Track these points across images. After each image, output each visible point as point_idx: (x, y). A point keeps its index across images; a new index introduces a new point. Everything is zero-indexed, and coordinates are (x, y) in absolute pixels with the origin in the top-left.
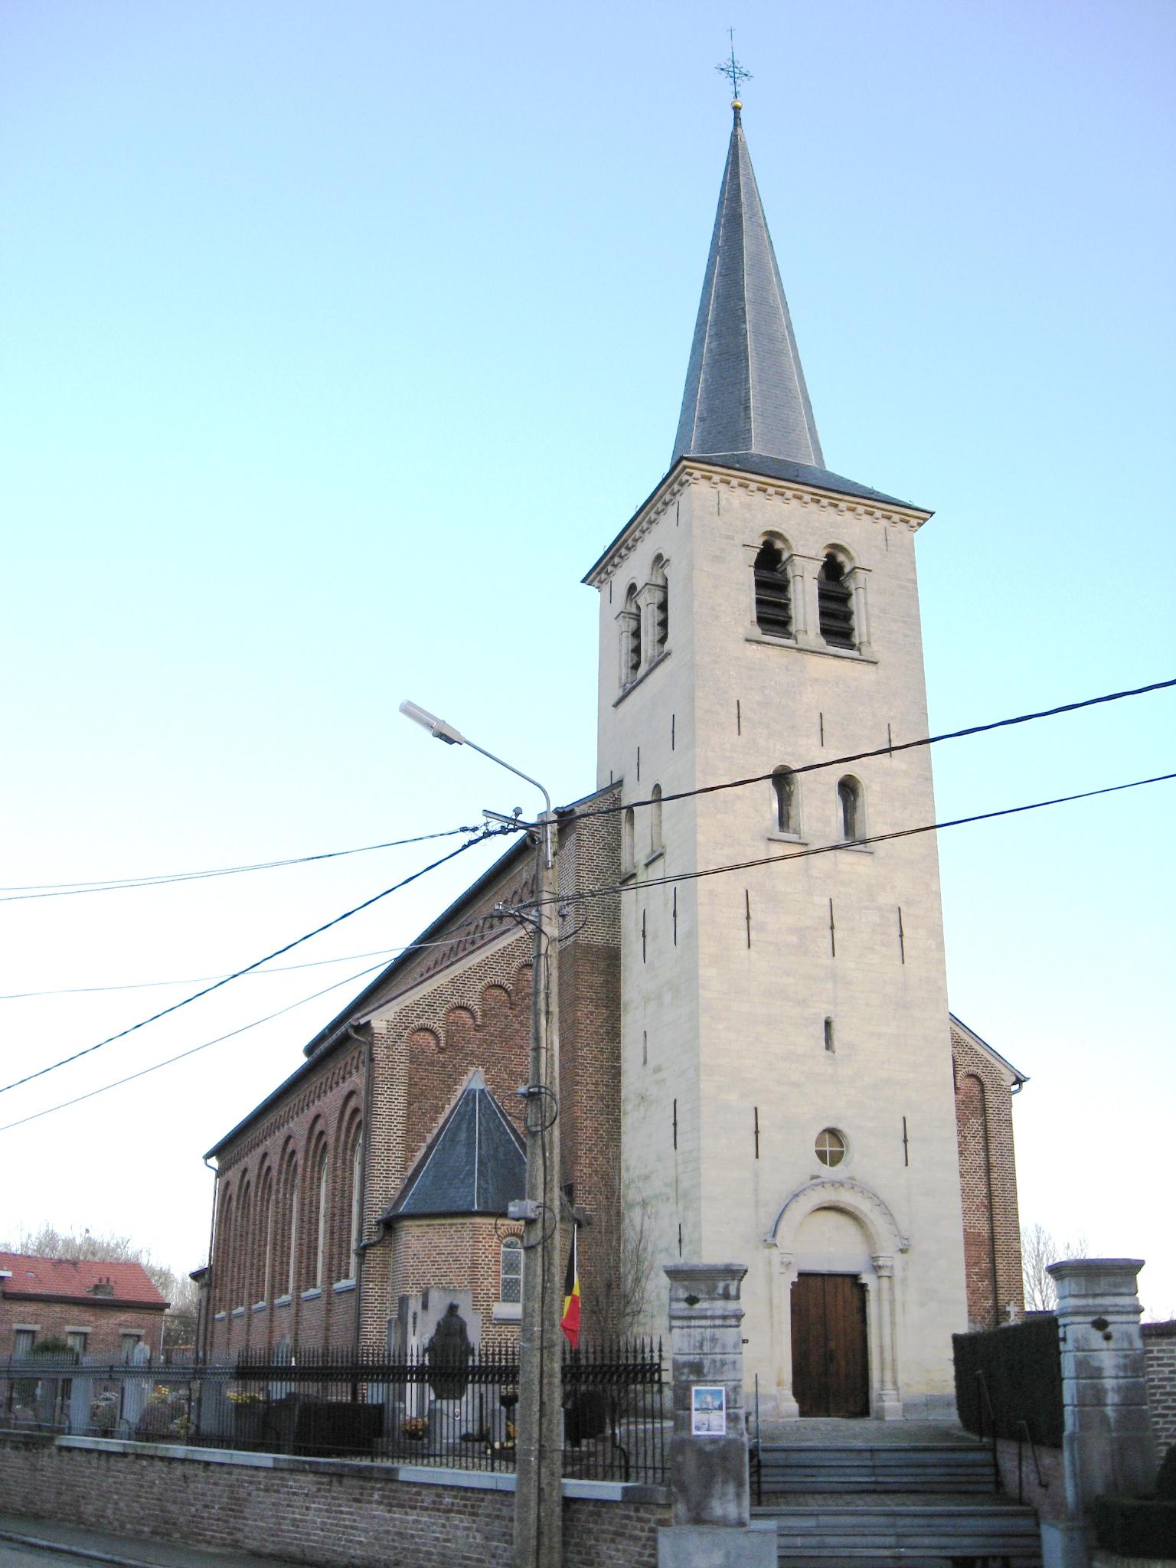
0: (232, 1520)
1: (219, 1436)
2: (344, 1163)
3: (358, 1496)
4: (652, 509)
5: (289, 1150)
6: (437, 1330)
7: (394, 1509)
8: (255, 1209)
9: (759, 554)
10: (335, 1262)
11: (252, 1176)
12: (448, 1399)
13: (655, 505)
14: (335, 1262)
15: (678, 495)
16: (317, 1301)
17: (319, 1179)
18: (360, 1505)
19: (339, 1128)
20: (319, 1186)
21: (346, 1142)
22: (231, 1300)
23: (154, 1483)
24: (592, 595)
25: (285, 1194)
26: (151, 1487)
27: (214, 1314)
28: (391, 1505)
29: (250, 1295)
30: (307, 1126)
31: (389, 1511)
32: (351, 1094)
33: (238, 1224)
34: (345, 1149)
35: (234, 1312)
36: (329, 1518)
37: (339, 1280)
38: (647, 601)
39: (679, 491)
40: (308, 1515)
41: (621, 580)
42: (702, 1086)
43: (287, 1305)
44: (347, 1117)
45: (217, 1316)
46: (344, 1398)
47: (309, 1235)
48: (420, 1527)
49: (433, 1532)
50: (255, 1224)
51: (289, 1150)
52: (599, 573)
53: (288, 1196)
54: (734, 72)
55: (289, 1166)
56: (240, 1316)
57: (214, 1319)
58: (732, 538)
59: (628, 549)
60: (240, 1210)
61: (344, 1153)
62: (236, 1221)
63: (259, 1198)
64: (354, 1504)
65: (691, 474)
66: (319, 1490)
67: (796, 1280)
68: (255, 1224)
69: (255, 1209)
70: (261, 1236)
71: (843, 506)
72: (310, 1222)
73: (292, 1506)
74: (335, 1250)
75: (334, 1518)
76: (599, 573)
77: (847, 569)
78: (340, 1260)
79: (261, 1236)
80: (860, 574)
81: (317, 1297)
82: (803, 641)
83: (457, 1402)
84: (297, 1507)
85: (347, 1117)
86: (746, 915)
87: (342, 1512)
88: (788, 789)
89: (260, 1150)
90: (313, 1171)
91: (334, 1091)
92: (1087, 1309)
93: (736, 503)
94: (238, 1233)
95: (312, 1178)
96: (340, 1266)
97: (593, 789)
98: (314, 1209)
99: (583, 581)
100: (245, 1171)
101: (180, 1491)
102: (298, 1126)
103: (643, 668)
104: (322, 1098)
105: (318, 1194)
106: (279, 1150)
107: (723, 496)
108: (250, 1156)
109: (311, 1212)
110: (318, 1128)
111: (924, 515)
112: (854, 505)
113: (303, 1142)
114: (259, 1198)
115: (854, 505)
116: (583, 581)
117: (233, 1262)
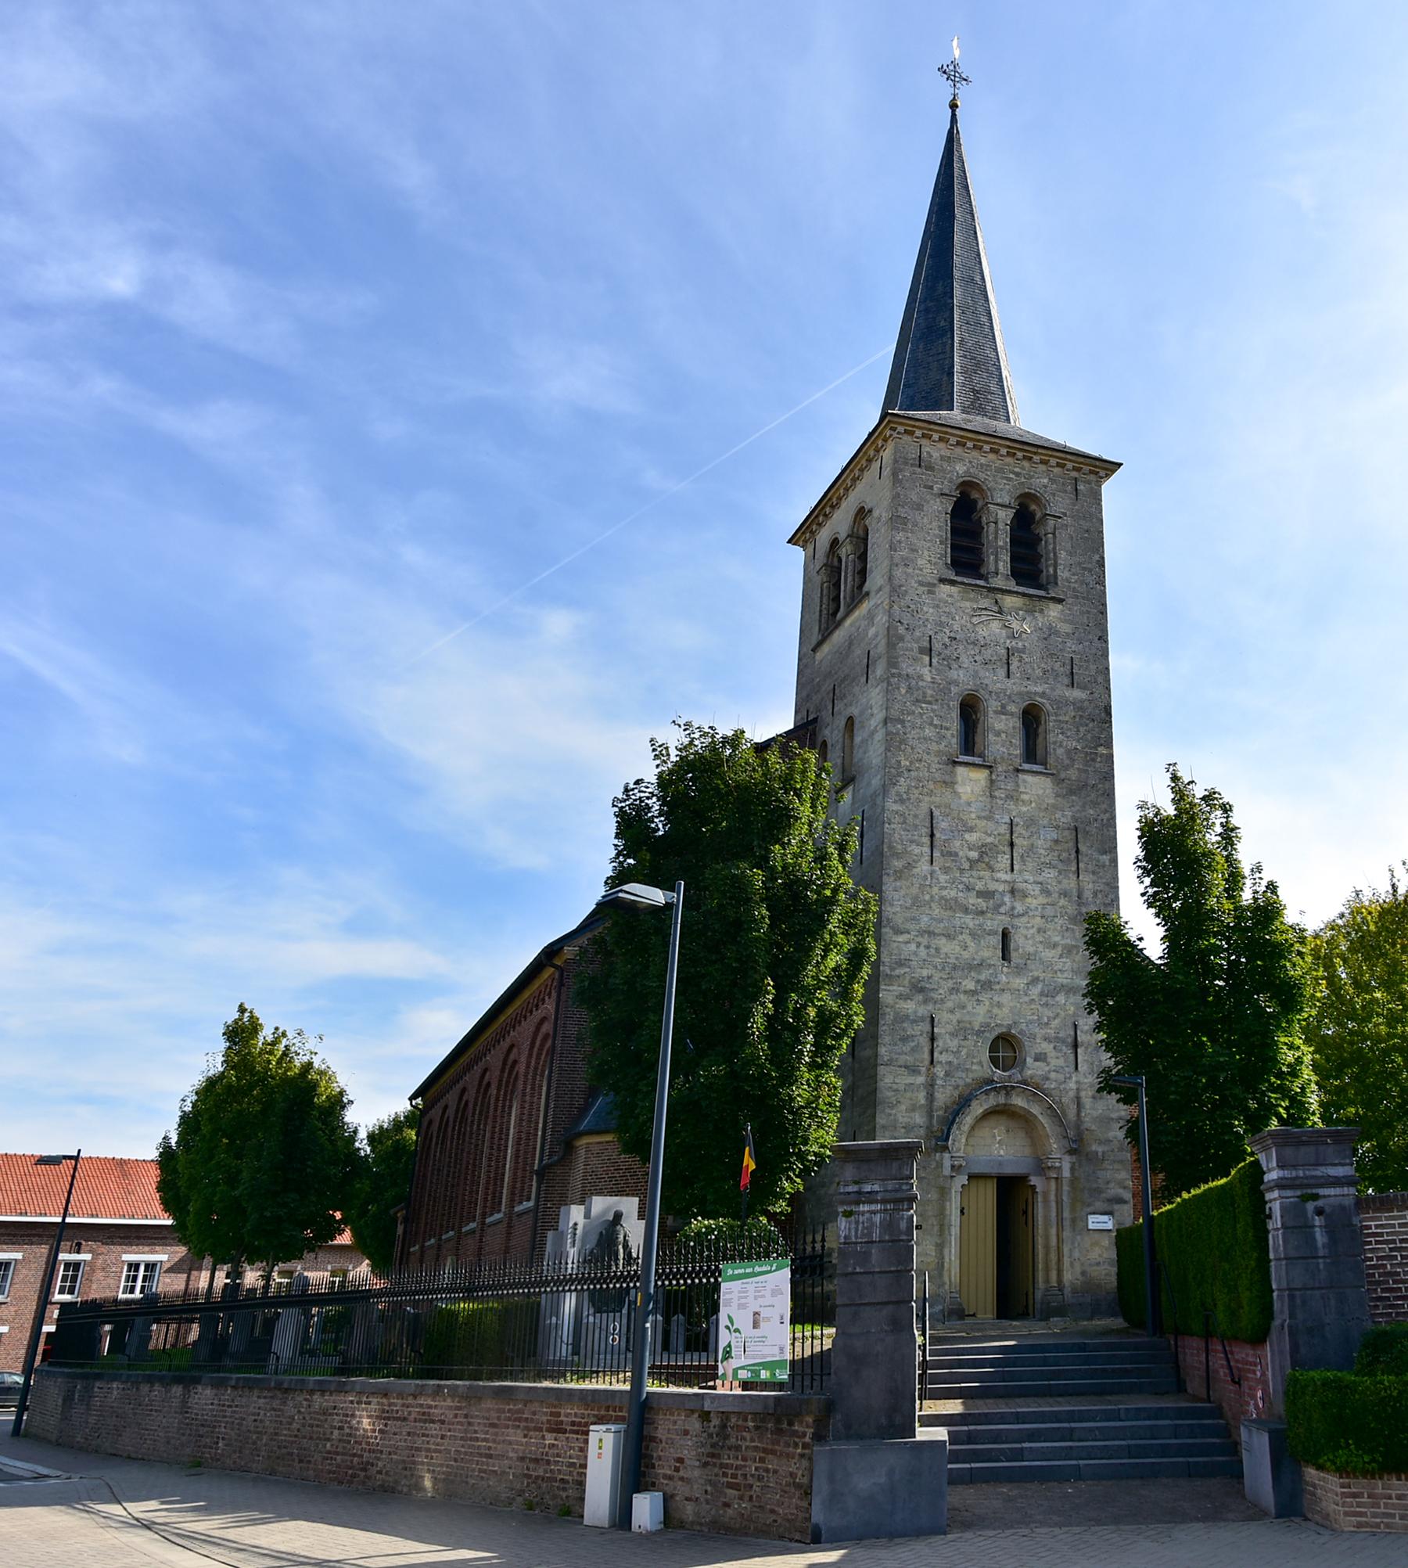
0: (366, 1454)
1: (98, 1377)
2: (533, 1089)
3: (496, 1421)
4: (856, 465)
5: (485, 1083)
6: (599, 1241)
7: (531, 1433)
8: (452, 1143)
9: (955, 502)
10: (518, 1185)
11: (451, 1112)
12: (607, 1312)
13: (858, 462)
14: (518, 1185)
15: (882, 452)
16: (500, 1226)
17: (511, 1107)
18: (496, 1430)
19: (530, 1055)
20: (510, 1114)
21: (536, 1068)
22: (425, 1232)
23: (294, 1419)
24: (798, 554)
25: (479, 1126)
26: (290, 1424)
27: (410, 1248)
28: (527, 1428)
29: (442, 1226)
30: (502, 1057)
31: (525, 1436)
32: (543, 1020)
33: (437, 1158)
34: (535, 1074)
35: (427, 1244)
36: (463, 1446)
37: (521, 1203)
38: (846, 551)
39: (882, 446)
40: (442, 1445)
41: (824, 536)
42: (881, 995)
43: (473, 1231)
44: (538, 1043)
45: (412, 1250)
46: (818, 1333)
47: (497, 1161)
48: (556, 1451)
49: (570, 1457)
50: (450, 1158)
51: (485, 1083)
52: (803, 533)
53: (482, 1127)
54: (951, 73)
55: (484, 1098)
56: (432, 1246)
57: (409, 1252)
58: (931, 488)
59: (833, 507)
60: (439, 1146)
61: (534, 1078)
62: (435, 1156)
63: (456, 1132)
64: (491, 1430)
65: (894, 429)
66: (456, 1416)
67: (1173, 796)
68: (450, 1158)
69: (452, 1143)
70: (455, 1167)
71: (1036, 458)
72: (499, 1149)
73: (427, 1436)
74: (519, 1173)
75: (470, 1447)
76: (802, 536)
77: (1038, 515)
78: (523, 1182)
79: (455, 1167)
80: (1051, 522)
81: (499, 1222)
82: (998, 582)
83: (618, 1314)
84: (432, 1436)
85: (538, 1043)
86: (930, 833)
87: (477, 1439)
88: (974, 717)
89: (459, 1086)
90: (505, 1100)
91: (528, 1020)
92: (1298, 1182)
93: (936, 455)
94: (436, 1167)
95: (503, 1106)
96: (522, 1189)
97: (791, 726)
98: (503, 1137)
99: (789, 542)
100: (446, 1107)
101: (317, 1426)
102: (494, 1059)
103: (839, 616)
104: (517, 1028)
105: (509, 1122)
106: (476, 1083)
107: (925, 449)
108: (451, 1092)
109: (500, 1139)
110: (512, 1057)
111: (1113, 467)
112: (1047, 458)
113: (498, 1073)
114: (456, 1132)
115: (1047, 458)
116: (789, 542)
117: (430, 1195)
